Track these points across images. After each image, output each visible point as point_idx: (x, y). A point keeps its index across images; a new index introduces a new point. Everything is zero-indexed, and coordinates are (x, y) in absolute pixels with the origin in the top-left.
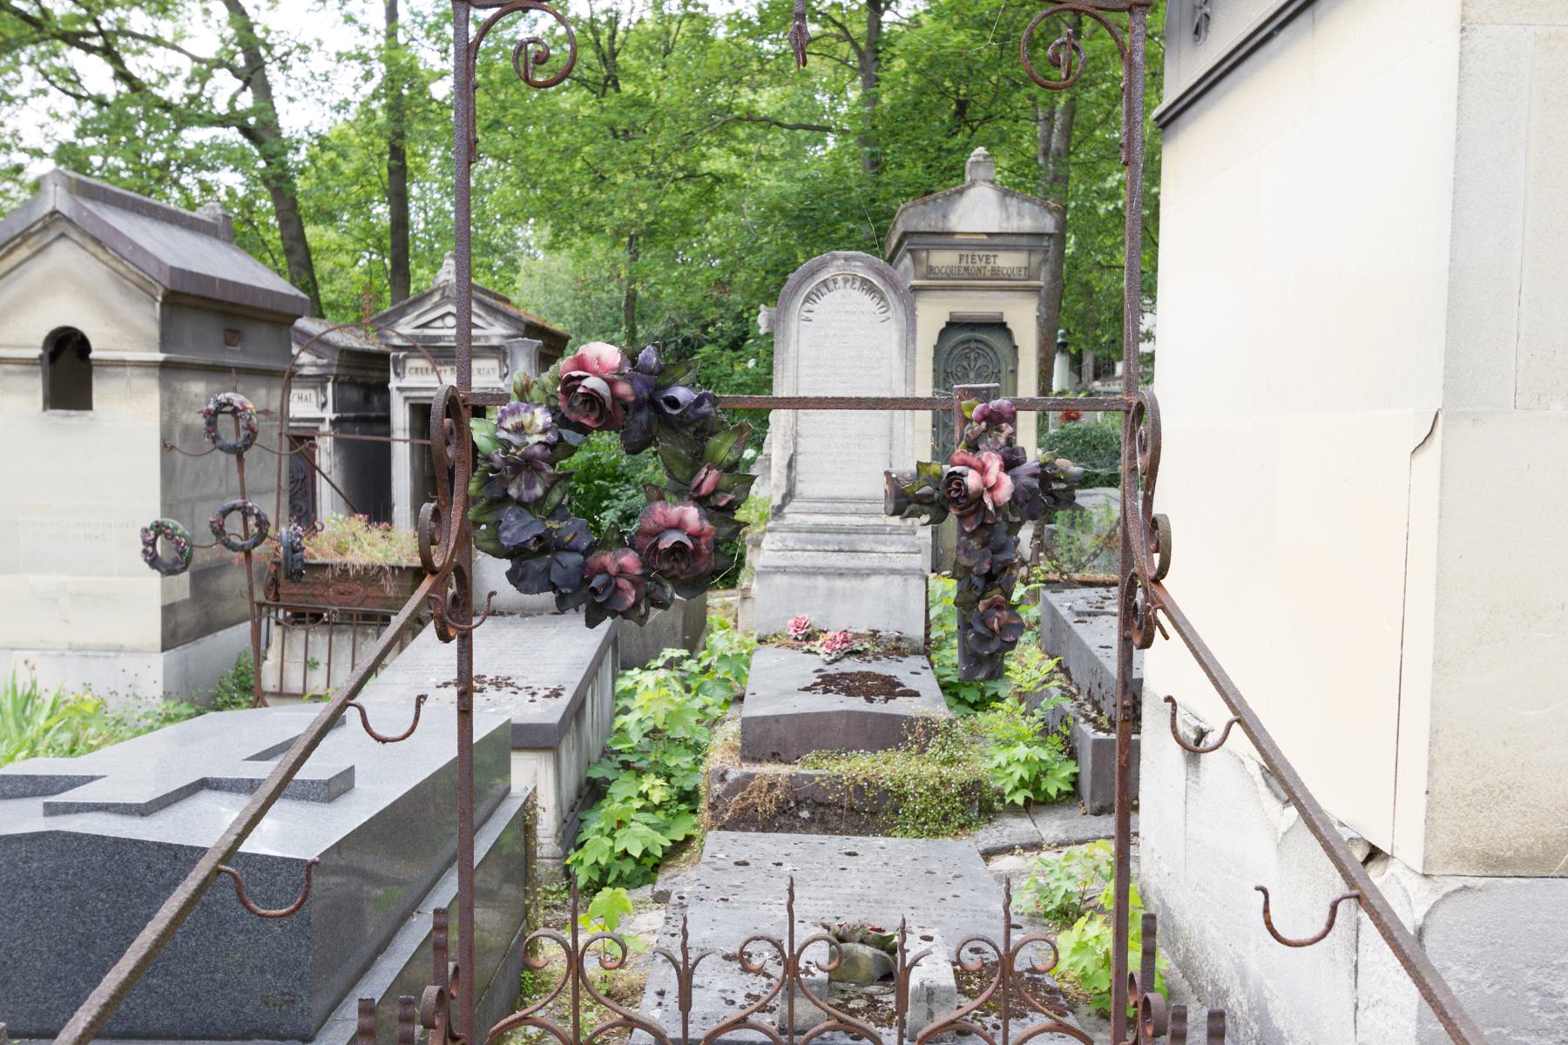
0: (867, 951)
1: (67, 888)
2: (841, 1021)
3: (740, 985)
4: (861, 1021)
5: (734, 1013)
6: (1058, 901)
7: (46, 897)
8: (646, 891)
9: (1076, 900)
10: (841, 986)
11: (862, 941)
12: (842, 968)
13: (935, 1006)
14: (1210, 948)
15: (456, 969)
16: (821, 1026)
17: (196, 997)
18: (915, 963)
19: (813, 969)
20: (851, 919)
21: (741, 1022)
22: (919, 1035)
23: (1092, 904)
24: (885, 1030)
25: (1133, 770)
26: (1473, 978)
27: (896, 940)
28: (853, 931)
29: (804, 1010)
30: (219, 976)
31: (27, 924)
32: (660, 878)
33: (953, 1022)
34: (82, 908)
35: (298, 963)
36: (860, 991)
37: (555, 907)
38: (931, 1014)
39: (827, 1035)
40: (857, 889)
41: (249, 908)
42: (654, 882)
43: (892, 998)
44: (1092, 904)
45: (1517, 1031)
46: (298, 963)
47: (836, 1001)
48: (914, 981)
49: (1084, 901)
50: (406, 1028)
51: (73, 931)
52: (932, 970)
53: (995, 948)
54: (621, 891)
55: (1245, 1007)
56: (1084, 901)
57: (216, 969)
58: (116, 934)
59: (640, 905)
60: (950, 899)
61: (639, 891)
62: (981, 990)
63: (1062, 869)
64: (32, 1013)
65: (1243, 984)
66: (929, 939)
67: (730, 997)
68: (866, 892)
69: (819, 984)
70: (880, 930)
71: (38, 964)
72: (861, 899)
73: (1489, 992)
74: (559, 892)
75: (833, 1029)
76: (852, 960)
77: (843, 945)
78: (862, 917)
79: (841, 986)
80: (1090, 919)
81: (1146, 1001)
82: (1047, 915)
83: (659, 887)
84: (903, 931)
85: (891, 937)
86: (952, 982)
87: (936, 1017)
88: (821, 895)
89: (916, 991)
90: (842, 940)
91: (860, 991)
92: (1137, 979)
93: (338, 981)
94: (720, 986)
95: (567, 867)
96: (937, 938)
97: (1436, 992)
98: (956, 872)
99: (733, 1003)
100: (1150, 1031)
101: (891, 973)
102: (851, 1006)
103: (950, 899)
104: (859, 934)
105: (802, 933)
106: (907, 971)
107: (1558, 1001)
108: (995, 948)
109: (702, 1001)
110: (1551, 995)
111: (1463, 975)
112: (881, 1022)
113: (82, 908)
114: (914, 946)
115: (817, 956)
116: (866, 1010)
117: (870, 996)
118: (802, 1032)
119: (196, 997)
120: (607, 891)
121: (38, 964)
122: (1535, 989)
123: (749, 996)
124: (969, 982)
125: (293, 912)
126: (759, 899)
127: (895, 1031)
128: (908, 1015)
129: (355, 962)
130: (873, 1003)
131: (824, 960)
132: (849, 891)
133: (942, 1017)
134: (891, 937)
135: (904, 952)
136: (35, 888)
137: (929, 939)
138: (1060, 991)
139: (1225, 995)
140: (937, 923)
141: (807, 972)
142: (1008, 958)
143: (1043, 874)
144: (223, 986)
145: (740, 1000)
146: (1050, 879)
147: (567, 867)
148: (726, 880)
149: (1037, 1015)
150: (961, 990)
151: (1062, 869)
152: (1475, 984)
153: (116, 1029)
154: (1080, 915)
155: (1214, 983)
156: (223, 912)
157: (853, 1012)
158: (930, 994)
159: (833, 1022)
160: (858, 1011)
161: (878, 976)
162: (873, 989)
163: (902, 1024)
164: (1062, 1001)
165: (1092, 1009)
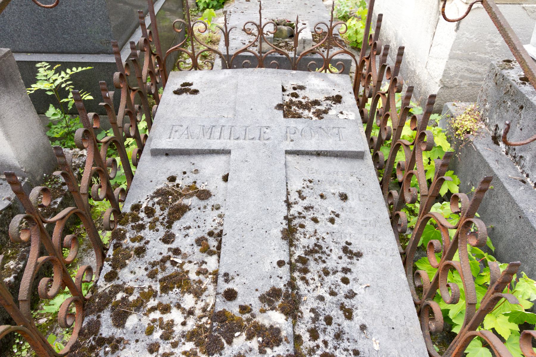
0: (285, 28)
1: (27, 5)
2: (276, 50)
3: (248, 39)
4: (283, 50)
5: (244, 47)
6: (343, 14)
7: (21, 8)
8: (221, 11)
9: (348, 14)
10: (277, 39)
11: (284, 25)
12: (278, 34)
13: (305, 45)
14: (387, 28)
15: (150, 32)
16: (270, 51)
17: (79, 41)
18: (300, 32)
19: (269, 33)
20: (281, 18)
21: (245, 50)
22: (301, 54)
23: (353, 15)
24: (290, 52)
25: (34, 277)
26: (471, 37)
27: (295, 25)
28: (281, 22)
29: (265, 46)
30: (85, 35)
31: (19, 17)
32: (225, 7)
33: (312, 50)
34: (35, 12)
35: (108, 31)
36: (283, 40)
37: (195, 16)
38: (304, 48)
39: (273, 53)
40: (283, 9)
41: (37, 4)
42: (223, 8)
43: (293, 43)
44: (353, 15)
45: (479, 53)
46: (108, 31)
47: (276, 43)
48: (300, 37)
49: (350, 14)
50: (134, 51)
51: (34, 20)
52: (306, 34)
53: (327, 26)
54: (212, 10)
55: (395, 46)
56: (350, 14)
57: (83, 33)
58: (48, 21)
59: (219, 15)
60: (311, 12)
61: (219, 11)
62: (320, 41)
63: (345, 3)
64: (31, 46)
65: (396, 39)
66: (305, 24)
67: (244, 42)
68: (286, 10)
69: (270, 38)
70: (290, 22)
71: (27, 31)
72: (285, 12)
73: (475, 41)
74: (195, 11)
75: (275, 52)
76: (281, 31)
77: (278, 26)
78: (284, 18)
79: (277, 39)
80: (353, 19)
81: (375, 43)
82: (339, 18)
83: (225, 9)
84: (298, 22)
85: (293, 24)
86: (311, 38)
87: (306, 49)
88: (272, 11)
89: (300, 40)
90: (278, 25)
91: (283, 40)
92: (373, 36)
93: (124, 37)
94: (241, 39)
95: (197, 3)
96: (307, 24)
97: (513, 39)
98: (314, 4)
99: (245, 44)
100: (375, 53)
101: (292, 35)
102: (280, 45)
103: (311, 12)
104: (283, 23)
105: (264, 22)
106: (298, 34)
107: (495, 44)
108: (327, 26)
109: (232, 44)
110: (493, 42)
111: (468, 36)
112: (289, 50)
113: (35, 12)
114: (300, 26)
115: (269, 29)
116: (285, 46)
117: (286, 42)
118: (265, 53)
119: (79, 41)
120: (208, 10)
121: (27, 31)
122: (489, 40)
123: (250, 42)
124: (316, 38)
125: (51, 7)
126: (253, 12)
127: (293, 52)
128: (297, 48)
129: (129, 31)
130: (287, 44)
131: (272, 30)
132: (280, 10)
133: (308, 49)
134: (293, 24)
135: (297, 28)
136: (17, 5)
137: (305, 24)
138: (343, 41)
139: (390, 42)
140: (307, 20)
141: (267, 34)
142: (331, 29)
143: (339, 6)
144: (87, 38)
145: (247, 43)
146: (341, 7)
147: (197, 3)
148: (243, 6)
149: (336, 48)
150: (314, 41)
151: (345, 3)
152: (471, 39)
153: (58, 51)
154: (349, 18)
155: (387, 39)
156: (80, 14)
157: (281, 47)
158: (304, 41)
159: (274, 50)
160: (282, 46)
161: (289, 36)
162: (287, 40)
163: (295, 51)
164: (343, 44)
165: (350, 46)
